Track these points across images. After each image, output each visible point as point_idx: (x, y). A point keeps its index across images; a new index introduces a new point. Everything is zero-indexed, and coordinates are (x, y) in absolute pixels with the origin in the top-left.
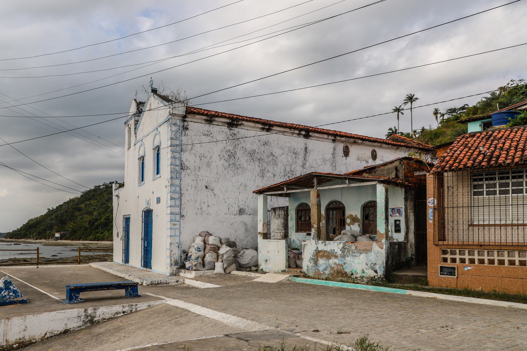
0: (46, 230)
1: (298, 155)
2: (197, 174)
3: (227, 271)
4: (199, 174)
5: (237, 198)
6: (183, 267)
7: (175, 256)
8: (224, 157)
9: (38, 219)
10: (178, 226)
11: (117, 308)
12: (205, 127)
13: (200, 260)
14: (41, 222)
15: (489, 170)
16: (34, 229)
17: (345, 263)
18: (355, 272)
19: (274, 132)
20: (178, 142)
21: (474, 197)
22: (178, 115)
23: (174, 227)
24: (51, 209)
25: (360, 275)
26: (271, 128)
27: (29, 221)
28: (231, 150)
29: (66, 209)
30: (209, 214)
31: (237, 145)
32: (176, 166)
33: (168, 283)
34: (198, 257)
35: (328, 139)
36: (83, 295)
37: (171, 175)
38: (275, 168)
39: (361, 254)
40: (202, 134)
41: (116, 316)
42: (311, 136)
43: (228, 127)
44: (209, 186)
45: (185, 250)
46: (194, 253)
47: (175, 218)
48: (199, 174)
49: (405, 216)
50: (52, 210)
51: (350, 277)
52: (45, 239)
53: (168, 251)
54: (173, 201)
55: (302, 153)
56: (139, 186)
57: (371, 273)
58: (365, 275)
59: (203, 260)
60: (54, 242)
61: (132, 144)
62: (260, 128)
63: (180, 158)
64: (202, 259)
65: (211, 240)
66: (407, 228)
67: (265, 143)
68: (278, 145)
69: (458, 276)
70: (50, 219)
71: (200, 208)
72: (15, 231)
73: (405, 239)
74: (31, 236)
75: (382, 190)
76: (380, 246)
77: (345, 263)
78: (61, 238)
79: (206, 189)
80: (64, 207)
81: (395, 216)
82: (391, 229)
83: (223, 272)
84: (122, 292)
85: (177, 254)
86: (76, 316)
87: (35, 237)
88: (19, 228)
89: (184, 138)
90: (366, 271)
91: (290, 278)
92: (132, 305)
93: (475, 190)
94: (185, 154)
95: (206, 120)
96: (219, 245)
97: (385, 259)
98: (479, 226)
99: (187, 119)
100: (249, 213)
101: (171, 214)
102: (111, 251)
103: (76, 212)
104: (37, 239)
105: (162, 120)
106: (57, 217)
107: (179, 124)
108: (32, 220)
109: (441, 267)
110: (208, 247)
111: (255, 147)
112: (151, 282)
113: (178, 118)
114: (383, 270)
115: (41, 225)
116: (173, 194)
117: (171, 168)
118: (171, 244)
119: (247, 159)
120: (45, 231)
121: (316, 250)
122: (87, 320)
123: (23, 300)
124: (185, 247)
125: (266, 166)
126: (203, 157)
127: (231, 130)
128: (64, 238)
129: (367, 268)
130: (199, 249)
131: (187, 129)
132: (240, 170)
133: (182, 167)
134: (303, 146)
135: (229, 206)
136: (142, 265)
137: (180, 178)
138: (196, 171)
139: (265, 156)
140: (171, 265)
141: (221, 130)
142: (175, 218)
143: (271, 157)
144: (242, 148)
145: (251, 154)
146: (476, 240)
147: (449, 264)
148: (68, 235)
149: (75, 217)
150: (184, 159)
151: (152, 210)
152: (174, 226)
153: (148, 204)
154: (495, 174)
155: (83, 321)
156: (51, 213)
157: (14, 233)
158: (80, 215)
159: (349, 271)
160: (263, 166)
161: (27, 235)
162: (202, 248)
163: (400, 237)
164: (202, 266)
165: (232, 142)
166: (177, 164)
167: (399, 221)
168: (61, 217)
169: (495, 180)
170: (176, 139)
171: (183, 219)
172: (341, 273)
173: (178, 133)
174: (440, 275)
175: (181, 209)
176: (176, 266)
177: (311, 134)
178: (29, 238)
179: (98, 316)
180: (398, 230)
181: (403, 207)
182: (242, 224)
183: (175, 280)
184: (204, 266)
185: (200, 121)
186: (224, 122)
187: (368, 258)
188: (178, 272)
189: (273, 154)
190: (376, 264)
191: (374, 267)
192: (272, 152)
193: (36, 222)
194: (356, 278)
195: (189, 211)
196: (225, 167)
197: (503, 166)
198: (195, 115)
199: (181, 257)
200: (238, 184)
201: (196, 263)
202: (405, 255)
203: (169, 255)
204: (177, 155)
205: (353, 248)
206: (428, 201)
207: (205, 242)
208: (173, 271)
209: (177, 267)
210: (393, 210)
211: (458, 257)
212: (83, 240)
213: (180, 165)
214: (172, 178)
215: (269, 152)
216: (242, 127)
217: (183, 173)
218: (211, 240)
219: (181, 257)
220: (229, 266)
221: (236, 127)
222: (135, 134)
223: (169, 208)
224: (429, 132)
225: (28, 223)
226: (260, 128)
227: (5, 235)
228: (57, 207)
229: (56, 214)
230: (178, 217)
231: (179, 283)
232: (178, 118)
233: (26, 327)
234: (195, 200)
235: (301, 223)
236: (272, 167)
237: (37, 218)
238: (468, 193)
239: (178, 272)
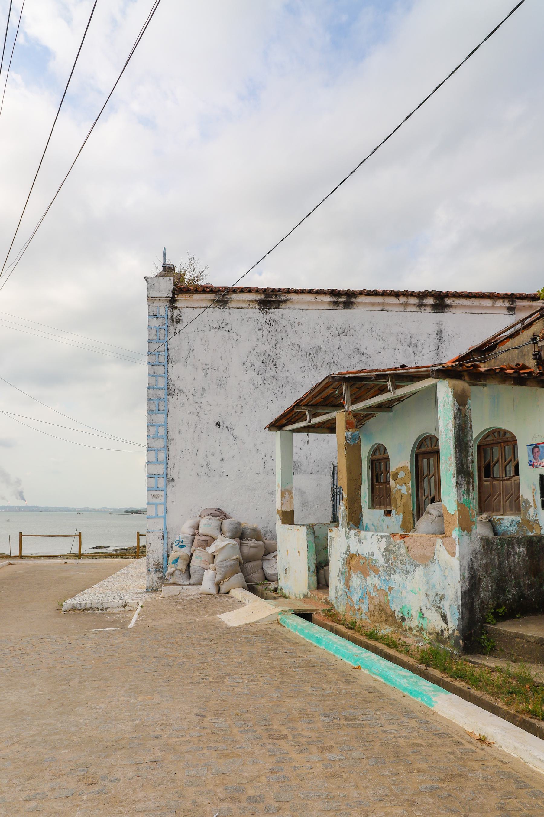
1: (420, 347)
3: (223, 589)
8: (252, 365)
13: (181, 565)
18: (408, 613)
19: (360, 307)
22: (160, 299)
23: (154, 500)
25: (417, 623)
26: (353, 300)
28: (268, 351)
30: (225, 474)
31: (281, 340)
32: (159, 389)
33: (107, 609)
34: (178, 559)
35: (493, 306)
37: (149, 407)
39: (416, 566)
40: (208, 328)
42: (449, 306)
43: (260, 309)
44: (223, 421)
47: (157, 483)
51: (400, 626)
54: (153, 453)
55: (433, 341)
58: (424, 624)
62: (329, 303)
63: (165, 375)
64: (186, 562)
67: (341, 331)
68: (372, 331)
71: (204, 464)
75: (447, 396)
76: (450, 550)
79: (216, 428)
82: (534, 501)
83: (214, 591)
85: (160, 551)
90: (427, 614)
91: (280, 617)
94: (175, 367)
97: (459, 586)
99: (178, 304)
100: (310, 471)
107: (163, 315)
111: (319, 341)
112: (73, 605)
113: (161, 304)
114: (457, 615)
116: (153, 440)
117: (148, 394)
119: (301, 365)
121: (346, 553)
126: (210, 370)
127: (266, 313)
129: (429, 606)
130: (181, 544)
132: (288, 387)
133: (170, 390)
134: (432, 329)
135: (265, 458)
137: (165, 412)
139: (342, 356)
140: (149, 571)
141: (247, 316)
142: (157, 483)
143: (357, 357)
144: (291, 346)
145: (312, 355)
150: (173, 376)
152: (154, 499)
164: (185, 576)
165: (269, 337)
166: (161, 386)
171: (173, 486)
172: (385, 612)
173: (162, 331)
175: (167, 468)
176: (158, 573)
177: (448, 301)
184: (189, 576)
186: (251, 301)
187: (428, 580)
189: (361, 351)
191: (441, 605)
192: (358, 346)
194: (411, 629)
196: (256, 384)
198: (190, 294)
204: (160, 370)
205: (403, 551)
208: (153, 582)
210: (536, 450)
213: (165, 387)
215: (352, 348)
216: (289, 305)
217: (172, 401)
220: (224, 579)
221: (278, 307)
226: (329, 303)
230: (162, 482)
231: (127, 608)
232: (162, 304)
235: (380, 487)
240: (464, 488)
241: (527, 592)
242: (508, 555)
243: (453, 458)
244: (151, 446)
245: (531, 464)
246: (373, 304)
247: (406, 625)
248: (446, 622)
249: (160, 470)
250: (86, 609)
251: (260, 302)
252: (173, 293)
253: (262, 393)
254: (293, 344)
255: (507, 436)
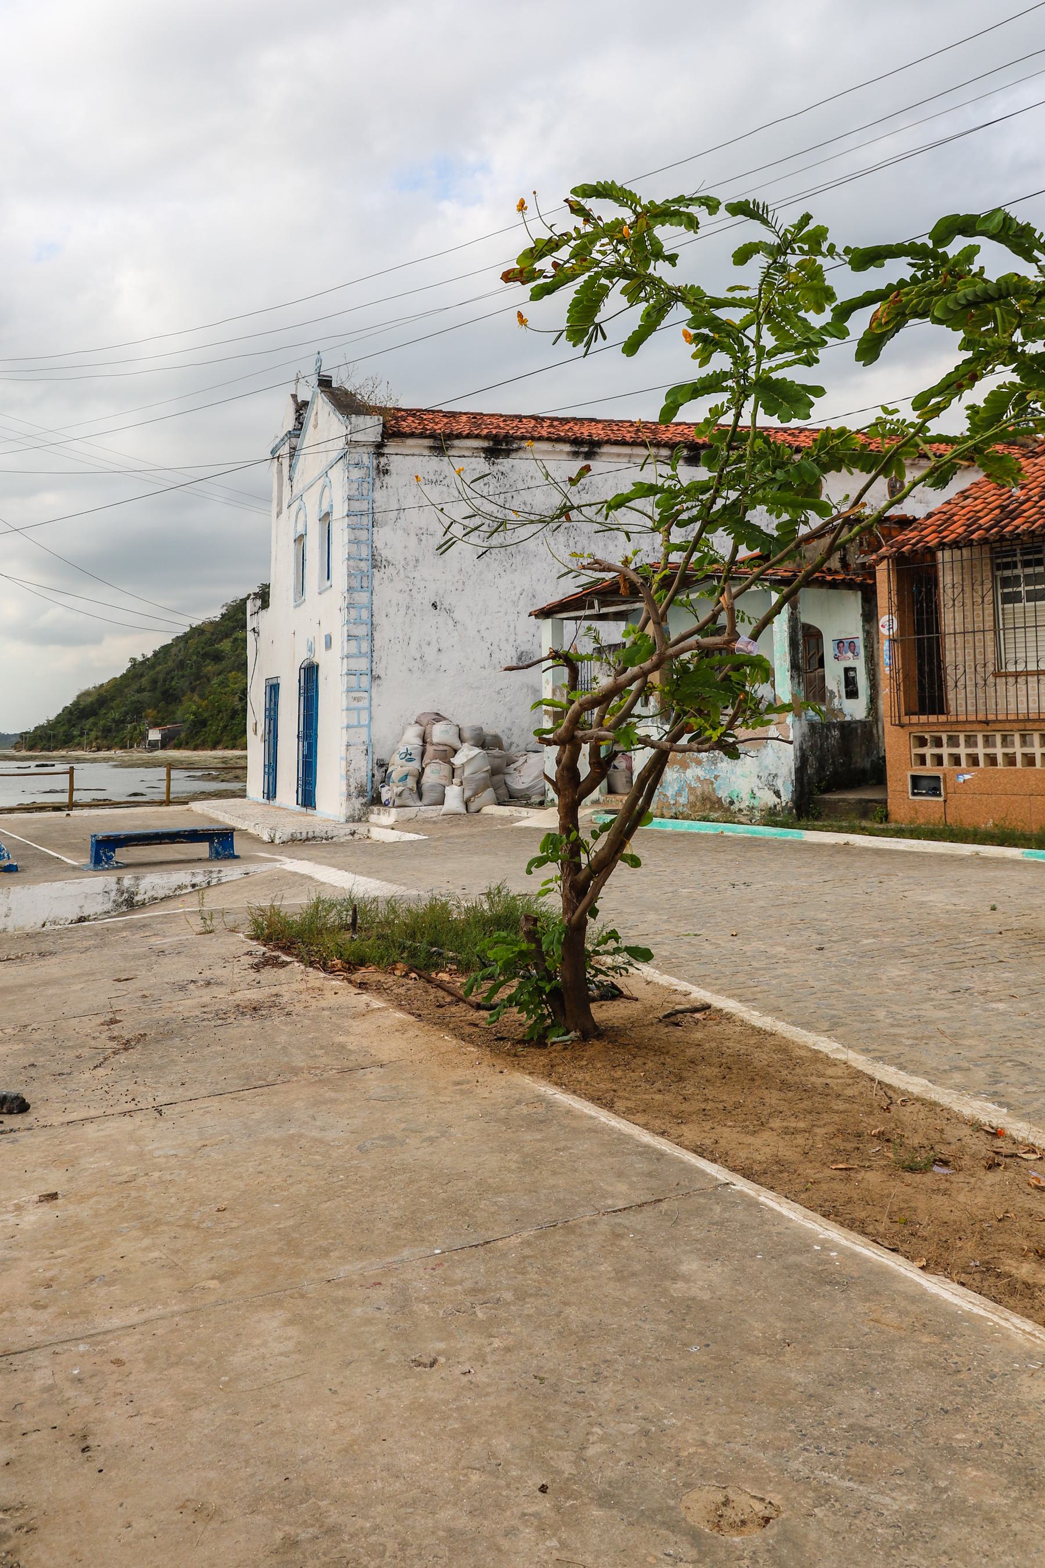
0: (123, 722)
2: (411, 575)
3: (473, 807)
4: (416, 574)
5: (512, 628)
6: (376, 800)
7: (357, 775)
9: (102, 691)
10: (365, 703)
11: (181, 877)
12: (430, 465)
13: (411, 782)
14: (113, 699)
15: (1001, 547)
16: (92, 720)
17: (716, 777)
19: (604, 458)
20: (364, 506)
21: (1006, 606)
23: (356, 704)
24: (140, 659)
27: (79, 697)
29: (180, 658)
30: (442, 669)
36: (122, 855)
37: (349, 583)
38: (611, 548)
41: (177, 893)
43: (485, 458)
45: (382, 760)
46: (398, 768)
47: (359, 681)
48: (416, 574)
49: (866, 657)
50: (143, 663)
51: (728, 810)
52: (121, 748)
53: (344, 763)
54: (353, 643)
56: (295, 607)
57: (768, 799)
58: (756, 803)
59: (418, 782)
60: (146, 755)
61: (285, 505)
62: (568, 453)
64: (416, 779)
65: (439, 733)
66: (874, 685)
69: (946, 796)
70: (135, 687)
71: (418, 656)
72: (43, 726)
73: (869, 714)
74: (85, 740)
77: (716, 777)
78: (165, 743)
79: (432, 609)
80: (174, 650)
81: (845, 659)
84: (202, 849)
85: (364, 769)
86: (100, 890)
87: (94, 744)
88: (52, 717)
89: (379, 495)
90: (758, 794)
92: (211, 872)
93: (1006, 590)
95: (431, 448)
96: (456, 743)
97: (793, 764)
98: (1038, 675)
99: (386, 450)
101: (348, 674)
102: (239, 772)
103: (208, 665)
104: (99, 749)
105: (334, 455)
106: (155, 682)
108: (86, 694)
109: (914, 778)
110: (430, 749)
113: (364, 449)
114: (791, 788)
115: (112, 708)
117: (348, 566)
118: (348, 745)
120: (120, 723)
122: (121, 900)
123: (10, 866)
124: (381, 754)
125: (586, 542)
128: (172, 743)
129: (761, 786)
131: (386, 472)
132: (519, 558)
133: (376, 562)
136: (300, 802)
138: (409, 568)
140: (349, 795)
142: (359, 681)
146: (1022, 709)
147: (929, 769)
148: (183, 735)
149: (205, 680)
150: (379, 544)
151: (317, 666)
153: (310, 650)
154: (1015, 555)
155: (114, 901)
156: (138, 670)
157: (39, 732)
158: (220, 674)
159: (724, 795)
160: (579, 545)
161: (74, 737)
162: (416, 754)
163: (856, 710)
164: (416, 796)
166: (364, 556)
167: (854, 669)
168: (165, 681)
169: (1016, 567)
170: (362, 497)
172: (710, 800)
173: (365, 485)
174: (911, 797)
178: (79, 746)
179: (142, 892)
180: (852, 693)
181: (860, 634)
182: (525, 690)
183: (348, 831)
184: (420, 796)
185: (416, 451)
188: (364, 814)
190: (776, 775)
193: (98, 700)
194: (740, 810)
195: (390, 665)
197: (1007, 540)
199: (373, 776)
200: (513, 593)
201: (401, 789)
202: (868, 754)
203: (344, 773)
204: (363, 535)
206: (880, 624)
207: (424, 739)
209: (364, 801)
211: (945, 751)
212: (226, 748)
213: (370, 557)
214: (350, 589)
216: (520, 454)
217: (378, 575)
218: (439, 733)
219: (373, 776)
220: (475, 794)
222: (291, 479)
223: (345, 660)
224: (860, 464)
225: (75, 704)
226: (568, 453)
227: (15, 740)
228: (156, 654)
229: (152, 673)
230: (365, 681)
231: (357, 836)
233: (10, 909)
234: (406, 638)
236: (601, 544)
237: (102, 685)
238: (954, 601)
239: (364, 814)
240: (796, 680)
241: (840, 770)
242: (827, 737)
243: (788, 655)
244: (352, 634)
245: (836, 658)
246: (619, 455)
247: (735, 808)
248: (779, 797)
249: (363, 664)
250: (308, 839)
251: (486, 450)
252: (383, 437)
253: (488, 565)
254: (525, 504)
255: (811, 630)
